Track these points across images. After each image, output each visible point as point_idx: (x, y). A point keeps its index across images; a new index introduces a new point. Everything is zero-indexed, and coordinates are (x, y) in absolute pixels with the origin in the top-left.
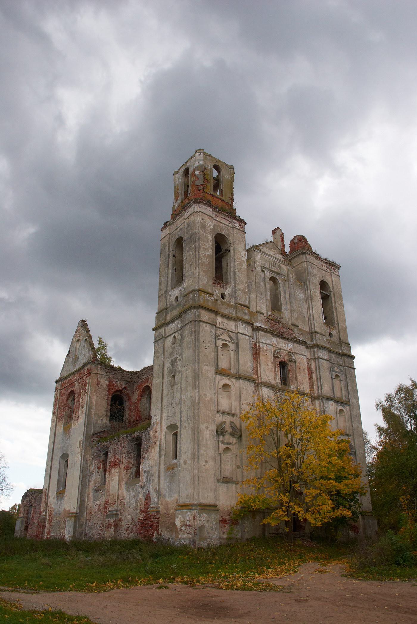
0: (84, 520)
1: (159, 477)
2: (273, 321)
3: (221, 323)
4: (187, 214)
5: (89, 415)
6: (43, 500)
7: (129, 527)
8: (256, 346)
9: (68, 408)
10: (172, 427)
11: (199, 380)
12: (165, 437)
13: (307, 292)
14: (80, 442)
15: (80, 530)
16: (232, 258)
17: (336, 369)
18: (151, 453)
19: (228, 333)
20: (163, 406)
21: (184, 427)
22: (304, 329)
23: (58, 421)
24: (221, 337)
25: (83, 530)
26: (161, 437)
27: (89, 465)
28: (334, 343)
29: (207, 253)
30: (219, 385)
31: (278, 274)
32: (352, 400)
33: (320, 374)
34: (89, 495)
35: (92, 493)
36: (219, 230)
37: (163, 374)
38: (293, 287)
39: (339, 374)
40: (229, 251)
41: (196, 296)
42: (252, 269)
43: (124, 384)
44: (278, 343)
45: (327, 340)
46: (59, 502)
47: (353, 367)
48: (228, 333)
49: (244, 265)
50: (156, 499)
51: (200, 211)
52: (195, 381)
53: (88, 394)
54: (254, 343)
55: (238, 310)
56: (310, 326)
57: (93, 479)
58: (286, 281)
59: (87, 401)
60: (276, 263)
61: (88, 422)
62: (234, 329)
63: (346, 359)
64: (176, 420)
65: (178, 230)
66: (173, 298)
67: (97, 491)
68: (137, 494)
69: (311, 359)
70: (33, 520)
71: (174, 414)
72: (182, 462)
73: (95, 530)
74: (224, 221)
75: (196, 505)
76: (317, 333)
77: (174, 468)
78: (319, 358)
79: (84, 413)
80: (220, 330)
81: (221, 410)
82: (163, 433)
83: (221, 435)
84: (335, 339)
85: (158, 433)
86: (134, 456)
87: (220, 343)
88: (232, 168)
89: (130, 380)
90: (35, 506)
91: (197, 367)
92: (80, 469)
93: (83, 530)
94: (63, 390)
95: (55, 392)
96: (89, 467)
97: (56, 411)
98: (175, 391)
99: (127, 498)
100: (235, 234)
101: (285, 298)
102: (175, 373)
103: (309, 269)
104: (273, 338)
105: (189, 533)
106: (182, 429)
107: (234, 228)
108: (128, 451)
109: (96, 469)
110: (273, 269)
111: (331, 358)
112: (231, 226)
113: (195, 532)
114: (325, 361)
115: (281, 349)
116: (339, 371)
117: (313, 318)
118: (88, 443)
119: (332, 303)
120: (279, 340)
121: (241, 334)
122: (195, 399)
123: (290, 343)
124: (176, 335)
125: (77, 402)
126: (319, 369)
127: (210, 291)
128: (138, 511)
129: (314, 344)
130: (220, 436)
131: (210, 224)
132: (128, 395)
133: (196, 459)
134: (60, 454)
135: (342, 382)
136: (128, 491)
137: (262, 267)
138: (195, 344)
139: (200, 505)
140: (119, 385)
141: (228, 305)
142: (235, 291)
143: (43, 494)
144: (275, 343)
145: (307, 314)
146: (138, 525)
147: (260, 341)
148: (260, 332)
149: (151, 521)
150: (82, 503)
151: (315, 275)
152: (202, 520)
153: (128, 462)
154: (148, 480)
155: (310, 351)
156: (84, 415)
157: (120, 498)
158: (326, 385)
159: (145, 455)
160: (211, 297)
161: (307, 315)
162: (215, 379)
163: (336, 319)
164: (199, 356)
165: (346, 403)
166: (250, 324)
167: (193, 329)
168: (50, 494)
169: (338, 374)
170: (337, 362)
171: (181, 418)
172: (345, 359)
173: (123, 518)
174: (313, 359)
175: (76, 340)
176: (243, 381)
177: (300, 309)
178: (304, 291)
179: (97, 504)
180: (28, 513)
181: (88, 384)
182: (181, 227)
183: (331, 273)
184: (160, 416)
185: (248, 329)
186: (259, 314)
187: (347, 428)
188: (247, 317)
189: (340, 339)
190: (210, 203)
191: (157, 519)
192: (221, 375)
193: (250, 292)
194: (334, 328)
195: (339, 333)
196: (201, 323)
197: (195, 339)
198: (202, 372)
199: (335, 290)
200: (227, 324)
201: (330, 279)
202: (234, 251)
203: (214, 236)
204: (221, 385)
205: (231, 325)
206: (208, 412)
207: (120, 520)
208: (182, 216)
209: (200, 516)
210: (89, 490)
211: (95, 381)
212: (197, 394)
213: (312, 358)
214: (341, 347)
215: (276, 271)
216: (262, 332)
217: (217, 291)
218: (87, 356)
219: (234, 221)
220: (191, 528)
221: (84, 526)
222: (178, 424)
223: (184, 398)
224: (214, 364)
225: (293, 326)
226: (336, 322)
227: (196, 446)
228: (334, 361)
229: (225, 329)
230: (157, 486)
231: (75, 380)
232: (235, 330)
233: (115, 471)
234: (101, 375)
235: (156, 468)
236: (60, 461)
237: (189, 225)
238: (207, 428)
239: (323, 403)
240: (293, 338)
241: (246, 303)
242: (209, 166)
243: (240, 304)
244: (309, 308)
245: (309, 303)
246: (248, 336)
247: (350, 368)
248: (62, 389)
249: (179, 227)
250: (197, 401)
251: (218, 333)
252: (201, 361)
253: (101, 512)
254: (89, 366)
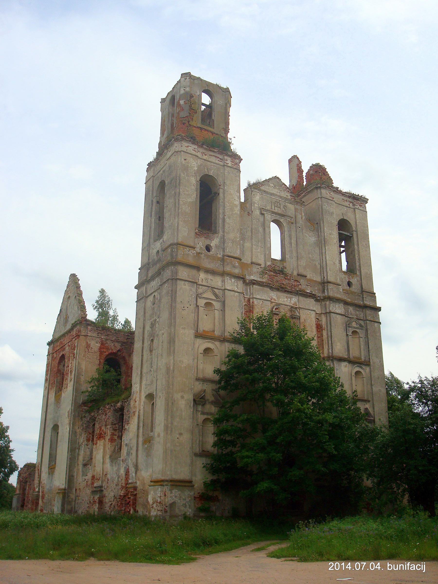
0: (73, 496)
1: (137, 451)
2: (272, 272)
3: (204, 280)
4: (169, 154)
5: (77, 382)
6: (37, 475)
7: (112, 504)
8: (250, 303)
9: (60, 374)
10: (150, 397)
11: (174, 345)
12: (144, 407)
13: (321, 234)
14: (68, 412)
15: (69, 507)
16: (222, 202)
17: (354, 324)
18: (131, 424)
19: (213, 291)
20: (143, 373)
21: (158, 396)
22: (314, 279)
23: (50, 388)
24: (203, 296)
25: (72, 508)
26: (140, 407)
27: (78, 437)
28: (353, 293)
29: (189, 200)
30: (199, 349)
31: (283, 216)
32: (374, 359)
33: (331, 332)
34: (78, 469)
35: (81, 467)
36: (206, 170)
37: (143, 338)
38: (302, 230)
39: (358, 330)
40: (219, 194)
41: (175, 250)
42: (248, 212)
43: (118, 346)
44: (278, 298)
45: (343, 290)
46: (50, 478)
47: (377, 320)
48: (213, 291)
49: (236, 210)
50: (134, 475)
51: (178, 151)
52: (170, 346)
53: (76, 359)
54: (247, 299)
55: (226, 263)
56: (322, 275)
57: (82, 453)
58: (292, 223)
59: (75, 367)
60: (281, 202)
61: (76, 390)
62: (221, 286)
63: (368, 312)
64: (152, 390)
65: (161, 172)
66: (155, 251)
67: (85, 465)
68: (118, 470)
69: (322, 313)
70: (28, 497)
71: (152, 382)
72: (156, 434)
73: (83, 507)
74: (213, 159)
75: (167, 481)
76: (330, 283)
77: (150, 441)
78: (330, 312)
79: (73, 380)
80: (203, 287)
81: (202, 377)
82: (142, 403)
83: (199, 404)
84: (355, 288)
85: (137, 403)
86: (119, 428)
87: (202, 302)
88: (227, 91)
89: (125, 341)
90: (30, 482)
91: (172, 331)
92: (69, 442)
93: (72, 508)
94: (55, 354)
95: (47, 356)
96: (78, 440)
97: (48, 377)
98: (153, 357)
99: (110, 473)
100: (226, 174)
101: (291, 243)
102: (154, 337)
103: (324, 207)
104: (272, 292)
105: (159, 510)
106: (157, 399)
107: (225, 167)
108: (113, 422)
109: (85, 442)
110: (276, 211)
111: (348, 311)
112: (222, 163)
113: (165, 509)
114: (338, 316)
115: (282, 304)
116: (358, 326)
117: (326, 265)
118: (77, 413)
119: (354, 245)
120: (280, 294)
121: (229, 290)
122: (170, 366)
123: (294, 296)
124: (156, 294)
125: (67, 367)
126: (331, 324)
127: (192, 244)
128: (120, 487)
129: (325, 296)
130: (199, 406)
131: (194, 164)
132: (124, 358)
133: (169, 432)
134: (52, 426)
135: (361, 339)
136: (112, 465)
137: (261, 209)
138: (171, 305)
139: (171, 481)
140: (113, 348)
141: (214, 258)
142: (223, 241)
143: (36, 469)
144: (274, 297)
145: (319, 261)
146: (119, 502)
147: (254, 296)
148: (254, 286)
149: (128, 498)
150: (70, 479)
151: (332, 213)
152: (174, 497)
153: (113, 434)
154: (128, 454)
155: (321, 305)
156: (72, 383)
157: (105, 473)
158: (338, 344)
159: (126, 427)
160: (192, 251)
161: (319, 262)
162: (194, 344)
163: (358, 264)
164: (175, 318)
165: (367, 363)
166: (241, 278)
167: (170, 289)
168: (43, 469)
169: (357, 330)
170: (356, 315)
171: (156, 386)
172: (367, 311)
173: (107, 495)
174: (324, 314)
175: (67, 299)
176: (229, 343)
177: (310, 256)
178: (317, 233)
179: (85, 480)
180: (24, 489)
181: (76, 348)
182: (164, 169)
183: (354, 209)
184: (139, 384)
185: (237, 284)
186: (254, 266)
187: (365, 393)
188: (237, 271)
189: (362, 288)
190: (194, 140)
191: (134, 495)
192: (202, 339)
193: (244, 240)
194: (355, 275)
195: (361, 280)
196: (178, 282)
197: (172, 300)
198: (178, 336)
199: (358, 230)
200: (211, 280)
201: (352, 216)
202: (224, 193)
203: (198, 179)
204: (201, 349)
205: (217, 282)
206: (184, 380)
207: (104, 496)
208: (164, 156)
209: (171, 493)
210: (78, 464)
211: (84, 344)
212: (172, 361)
213: (323, 312)
214: (363, 298)
215: (280, 212)
216: (257, 287)
217: (201, 243)
218: (77, 315)
219: (226, 157)
220: (161, 505)
221: (74, 503)
222: (155, 394)
223: (160, 364)
224: (193, 326)
225: (299, 277)
226: (357, 267)
227: (169, 417)
228: (351, 314)
229: (210, 286)
230: (134, 460)
231: (66, 343)
232: (222, 287)
233: (101, 443)
234: (91, 336)
235: (134, 441)
236: (51, 432)
237: (170, 167)
238: (182, 397)
239: (333, 364)
240: (298, 291)
241: (237, 254)
242: (197, 92)
243: (229, 256)
244: (321, 254)
245: (322, 247)
246: (238, 292)
247: (373, 322)
248: (54, 353)
249: (162, 169)
250: (171, 369)
251: (200, 291)
252: (177, 324)
253: (88, 488)
254: (78, 327)
